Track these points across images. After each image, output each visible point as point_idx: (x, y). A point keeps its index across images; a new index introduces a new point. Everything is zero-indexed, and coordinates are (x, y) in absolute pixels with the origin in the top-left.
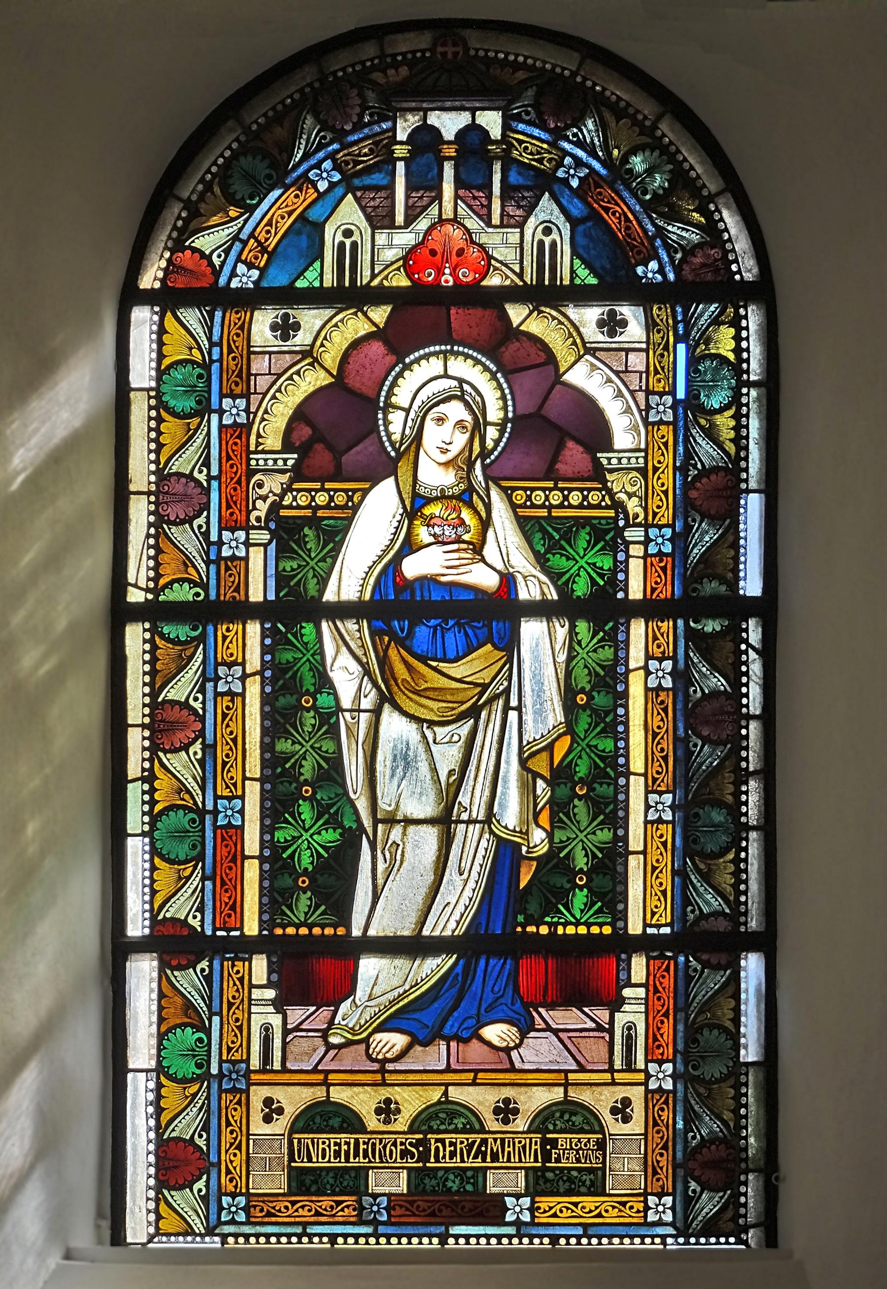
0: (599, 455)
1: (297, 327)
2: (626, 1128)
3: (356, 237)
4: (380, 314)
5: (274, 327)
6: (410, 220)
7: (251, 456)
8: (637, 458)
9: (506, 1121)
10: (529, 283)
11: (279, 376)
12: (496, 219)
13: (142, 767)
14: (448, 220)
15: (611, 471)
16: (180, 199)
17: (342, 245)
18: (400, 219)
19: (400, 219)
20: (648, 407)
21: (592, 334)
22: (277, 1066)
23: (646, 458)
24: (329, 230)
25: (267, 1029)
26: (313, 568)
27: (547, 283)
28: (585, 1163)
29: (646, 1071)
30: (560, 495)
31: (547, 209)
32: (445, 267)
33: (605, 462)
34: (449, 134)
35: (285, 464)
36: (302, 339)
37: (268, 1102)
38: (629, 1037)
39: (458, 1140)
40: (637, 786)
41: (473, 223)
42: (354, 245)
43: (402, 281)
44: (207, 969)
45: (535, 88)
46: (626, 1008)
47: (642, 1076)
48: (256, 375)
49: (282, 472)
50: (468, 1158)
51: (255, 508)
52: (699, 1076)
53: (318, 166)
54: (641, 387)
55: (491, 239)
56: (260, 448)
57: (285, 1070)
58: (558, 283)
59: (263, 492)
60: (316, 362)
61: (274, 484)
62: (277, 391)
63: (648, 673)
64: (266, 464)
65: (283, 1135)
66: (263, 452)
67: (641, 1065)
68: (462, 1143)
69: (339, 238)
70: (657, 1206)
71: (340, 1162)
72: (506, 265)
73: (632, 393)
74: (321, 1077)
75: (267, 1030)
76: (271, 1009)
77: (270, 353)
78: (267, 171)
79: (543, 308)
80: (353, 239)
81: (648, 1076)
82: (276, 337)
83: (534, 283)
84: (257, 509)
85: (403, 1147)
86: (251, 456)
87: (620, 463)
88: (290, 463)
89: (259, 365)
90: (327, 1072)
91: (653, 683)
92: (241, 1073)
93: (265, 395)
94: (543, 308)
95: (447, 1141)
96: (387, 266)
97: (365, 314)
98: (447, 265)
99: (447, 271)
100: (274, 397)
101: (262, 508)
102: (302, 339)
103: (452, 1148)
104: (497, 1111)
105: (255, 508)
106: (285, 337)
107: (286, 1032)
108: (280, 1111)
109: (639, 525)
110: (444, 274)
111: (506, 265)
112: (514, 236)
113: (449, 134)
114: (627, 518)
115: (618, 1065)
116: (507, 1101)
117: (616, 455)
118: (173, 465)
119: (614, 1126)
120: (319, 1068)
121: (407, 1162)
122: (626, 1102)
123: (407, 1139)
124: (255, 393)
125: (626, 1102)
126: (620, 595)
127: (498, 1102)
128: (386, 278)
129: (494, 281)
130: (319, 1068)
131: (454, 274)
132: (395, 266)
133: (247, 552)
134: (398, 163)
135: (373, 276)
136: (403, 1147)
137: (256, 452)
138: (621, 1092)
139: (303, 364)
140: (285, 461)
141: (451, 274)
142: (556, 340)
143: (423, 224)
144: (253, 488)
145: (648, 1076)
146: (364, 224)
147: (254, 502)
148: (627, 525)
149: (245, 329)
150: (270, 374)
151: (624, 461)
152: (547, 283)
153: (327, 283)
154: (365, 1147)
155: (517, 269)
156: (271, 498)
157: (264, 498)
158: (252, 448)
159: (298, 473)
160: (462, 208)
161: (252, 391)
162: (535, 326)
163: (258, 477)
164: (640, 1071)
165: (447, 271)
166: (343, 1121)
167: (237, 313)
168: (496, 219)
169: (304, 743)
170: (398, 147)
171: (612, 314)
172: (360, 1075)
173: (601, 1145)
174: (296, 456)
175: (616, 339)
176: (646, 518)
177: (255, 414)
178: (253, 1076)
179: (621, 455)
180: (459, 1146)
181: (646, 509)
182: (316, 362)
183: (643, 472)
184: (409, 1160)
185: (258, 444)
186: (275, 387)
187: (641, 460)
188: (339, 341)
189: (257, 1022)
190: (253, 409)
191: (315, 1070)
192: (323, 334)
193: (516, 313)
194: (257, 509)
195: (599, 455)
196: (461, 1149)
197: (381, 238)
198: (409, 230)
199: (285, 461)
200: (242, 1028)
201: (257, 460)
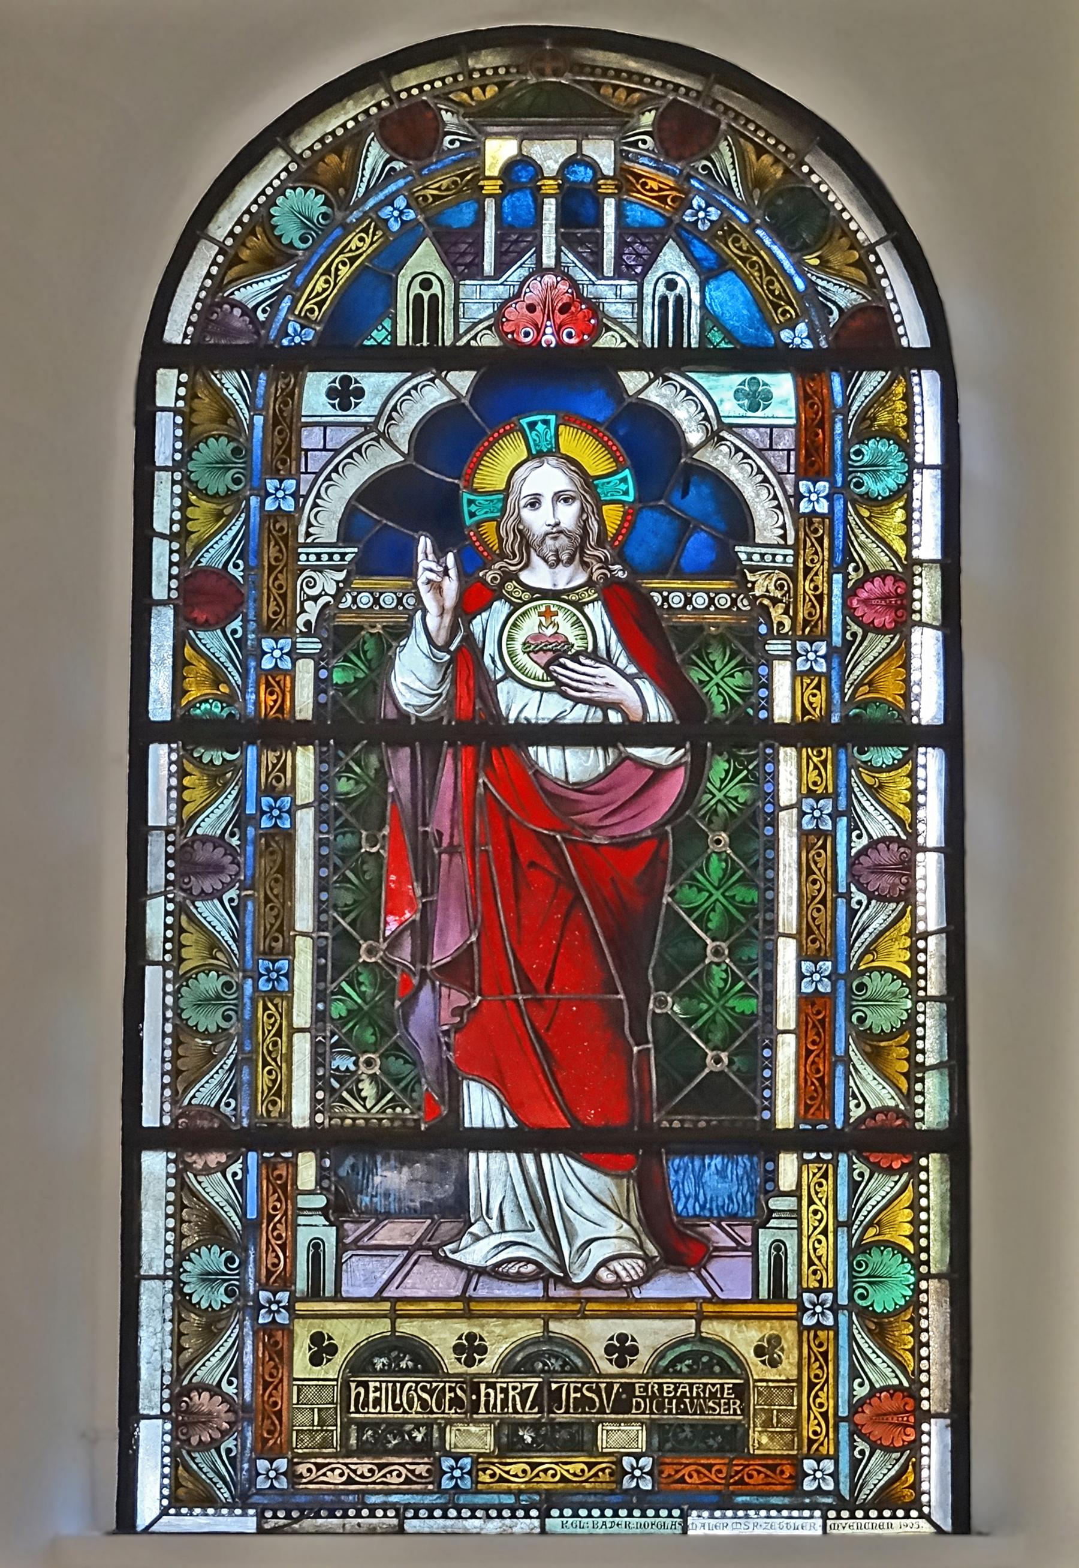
0: (737, 549)
1: (360, 393)
2: (771, 1374)
3: (436, 289)
4: (463, 380)
5: (331, 393)
6: (501, 268)
7: (300, 550)
8: (785, 556)
9: (470, 1362)
10: (649, 345)
11: (337, 452)
12: (608, 269)
13: (165, 923)
14: (549, 270)
15: (753, 570)
16: (213, 240)
17: (664, 300)
18: (488, 267)
19: (488, 267)
20: (799, 497)
21: (731, 409)
22: (330, 1289)
23: (796, 556)
24: (403, 283)
25: (316, 1246)
26: (718, 685)
27: (670, 345)
28: (695, 1413)
29: (799, 1302)
30: (705, 596)
31: (671, 258)
32: (546, 326)
33: (743, 557)
34: (551, 167)
35: (342, 559)
36: (366, 408)
37: (317, 1339)
38: (778, 1258)
39: (510, 1385)
40: (787, 951)
41: (582, 275)
42: (679, 299)
43: (489, 340)
44: (240, 1172)
45: (653, 113)
46: (773, 1223)
47: (793, 1308)
48: (307, 451)
49: (339, 569)
50: (523, 1407)
51: (303, 611)
52: (868, 1307)
53: (390, 201)
54: (789, 469)
55: (603, 290)
56: (309, 540)
57: (337, 1297)
58: (440, 344)
59: (313, 592)
60: (384, 437)
61: (328, 583)
62: (765, 476)
63: (802, 814)
64: (774, 561)
65: (336, 1380)
66: (313, 545)
67: (792, 1295)
68: (514, 1388)
69: (416, 289)
70: (815, 1471)
71: (380, 1413)
72: (620, 325)
73: (778, 474)
74: (387, 1306)
75: (778, 1249)
76: (321, 1220)
77: (325, 426)
78: (324, 209)
79: (671, 375)
80: (432, 291)
81: (290, 1308)
82: (333, 406)
83: (656, 346)
84: (305, 612)
85: (579, 1395)
86: (300, 550)
87: (331, 559)
88: (348, 558)
89: (311, 438)
90: (395, 1300)
91: (808, 824)
92: (828, 1305)
93: (318, 475)
94: (671, 375)
95: (372, 1385)
96: (475, 324)
97: (444, 380)
98: (548, 323)
99: (549, 330)
100: (328, 478)
101: (312, 611)
102: (366, 408)
103: (378, 1394)
104: (458, 1349)
105: (303, 611)
106: (345, 406)
107: (341, 1247)
108: (333, 1350)
109: (785, 636)
110: (544, 334)
111: (620, 325)
112: (629, 289)
113: (551, 167)
114: (770, 628)
115: (763, 1294)
116: (471, 1337)
117: (758, 550)
118: (202, 556)
119: (758, 1369)
120: (385, 1294)
121: (368, 1413)
122: (775, 1341)
123: (583, 1384)
124: (306, 473)
125: (775, 1341)
126: (915, 720)
127: (611, 1339)
128: (474, 338)
129: (608, 341)
130: (385, 1294)
131: (557, 332)
132: (486, 324)
133: (294, 664)
134: (607, 200)
135: (457, 336)
136: (579, 1395)
137: (305, 545)
138: (769, 1329)
139: (367, 438)
140: (343, 556)
141: (552, 334)
142: (684, 414)
143: (515, 274)
144: (302, 589)
145: (290, 1308)
146: (442, 272)
147: (302, 603)
148: (770, 635)
149: (292, 396)
150: (325, 449)
151: (768, 558)
152: (670, 345)
153: (401, 342)
154: (378, 1394)
155: (634, 328)
156: (322, 601)
157: (315, 599)
158: (301, 540)
159: (362, 568)
160: (568, 257)
161: (303, 470)
162: (658, 395)
163: (306, 573)
164: (790, 1302)
165: (549, 330)
166: (565, 1363)
167: (285, 377)
168: (608, 269)
169: (713, 899)
170: (486, 182)
171: (346, 381)
172: (740, 1306)
173: (741, 1392)
174: (356, 550)
175: (759, 413)
176: (793, 628)
177: (306, 497)
178: (299, 1306)
179: (763, 550)
180: (511, 1393)
181: (794, 619)
182: (384, 437)
183: (791, 573)
184: (371, 1410)
185: (308, 534)
186: (330, 468)
187: (790, 559)
188: (414, 414)
189: (304, 1237)
190: (303, 492)
191: (378, 1298)
192: (392, 403)
193: (632, 380)
194: (305, 612)
195: (737, 549)
196: (514, 1397)
197: (469, 287)
198: (499, 282)
199: (343, 556)
200: (288, 1246)
201: (308, 554)
